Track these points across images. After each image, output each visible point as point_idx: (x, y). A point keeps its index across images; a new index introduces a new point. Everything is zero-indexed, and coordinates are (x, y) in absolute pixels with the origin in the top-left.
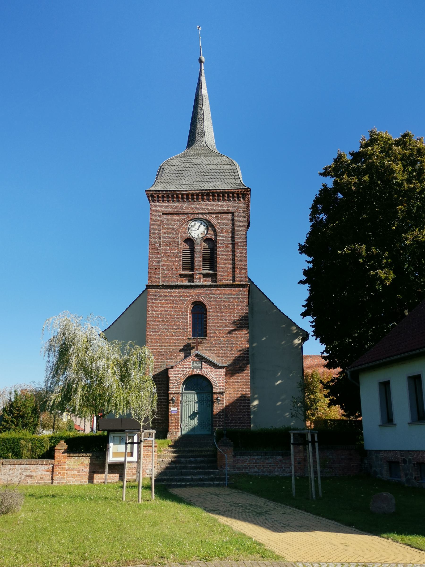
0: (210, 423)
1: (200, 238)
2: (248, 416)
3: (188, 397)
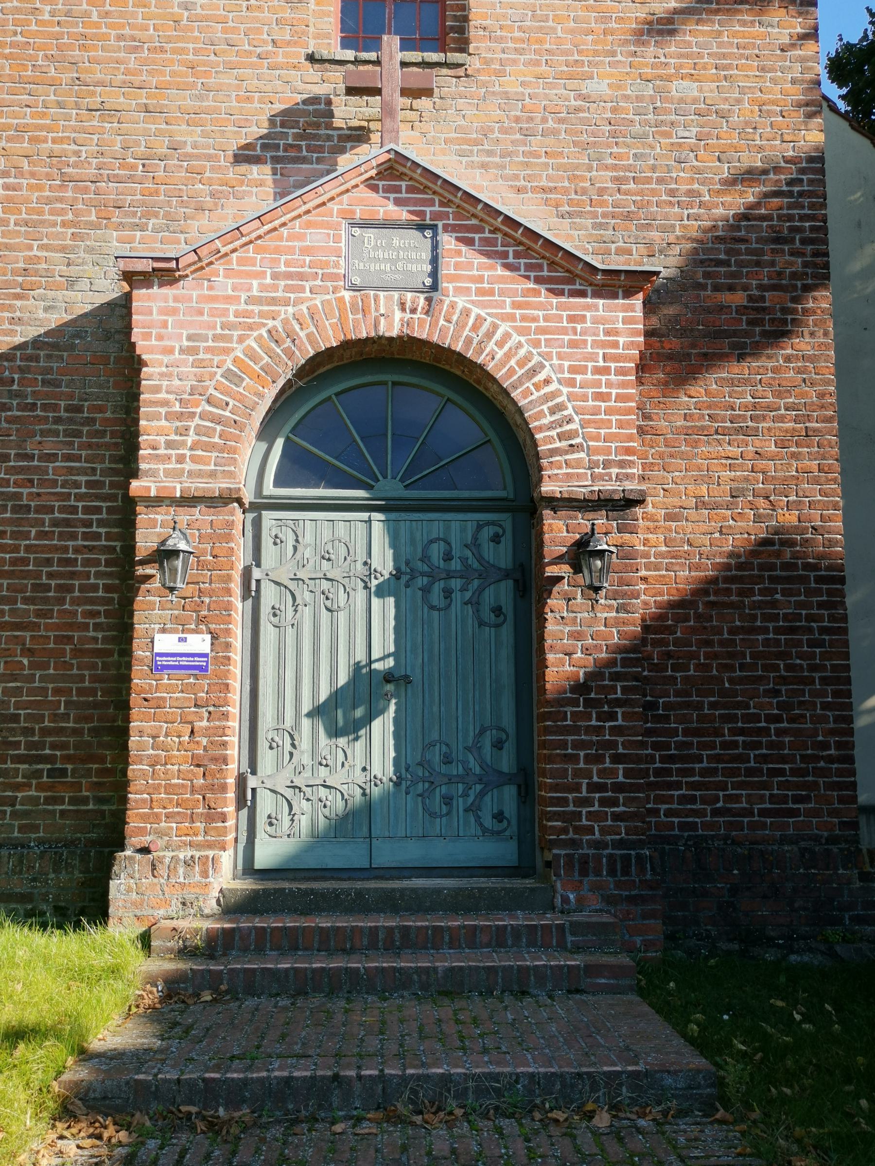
0: (507, 762)
2: (826, 706)
3: (308, 538)
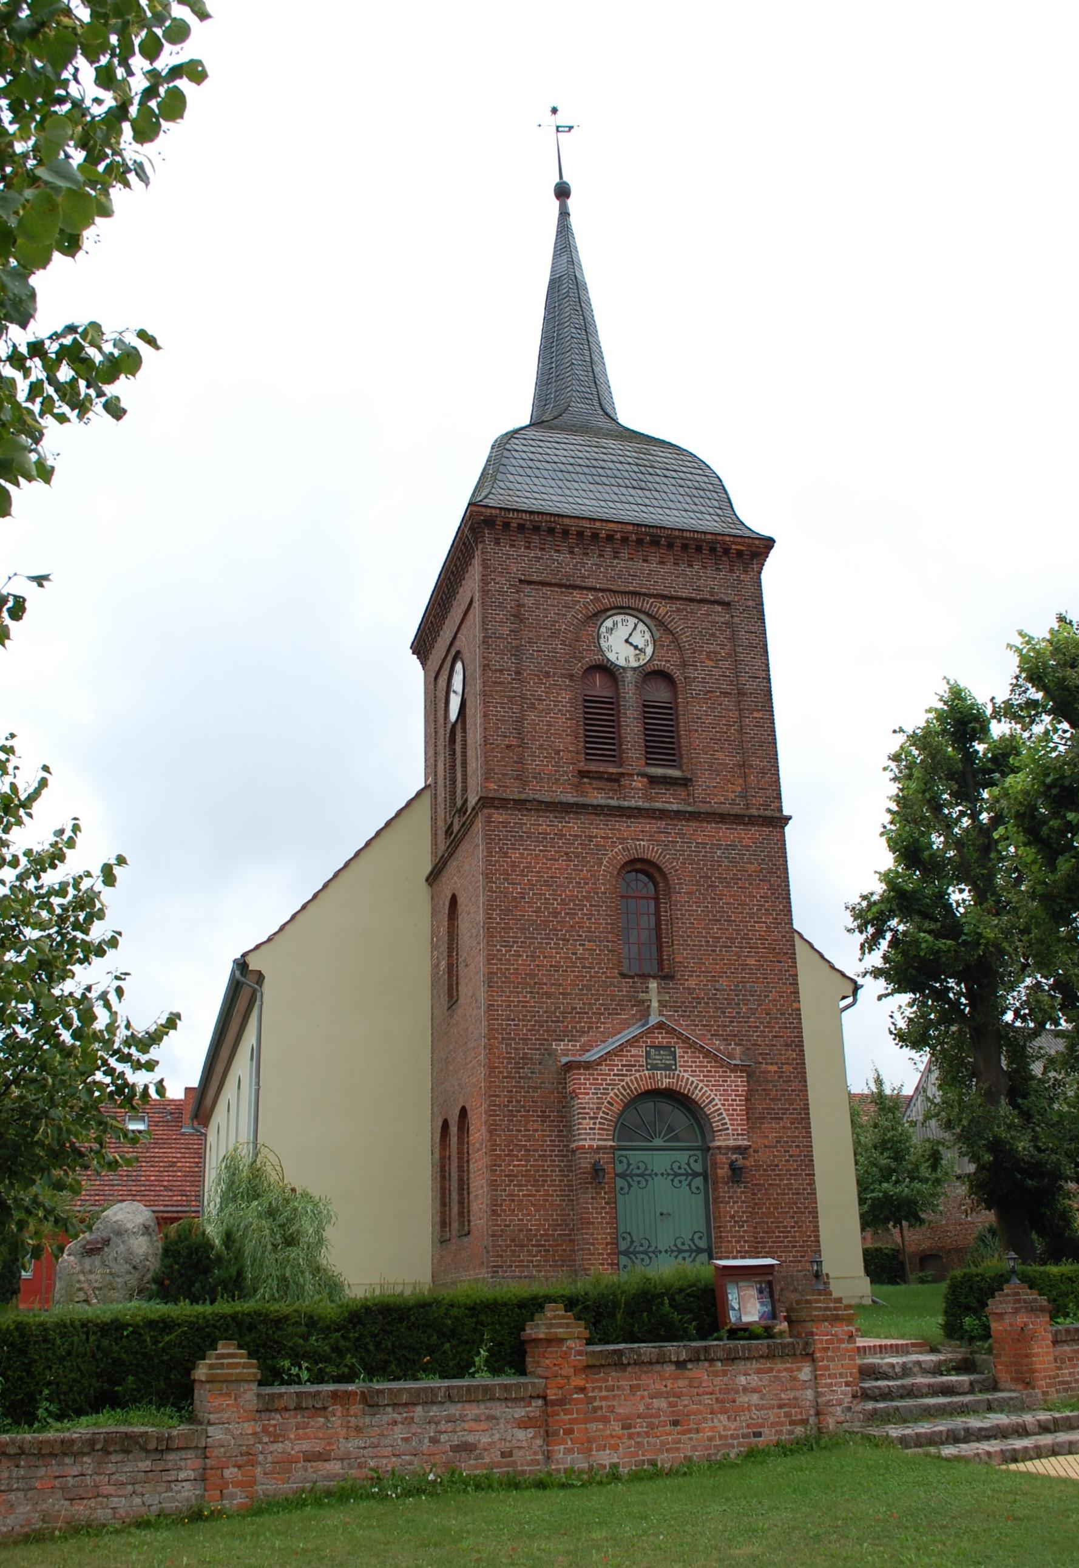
1: (634, 669)
